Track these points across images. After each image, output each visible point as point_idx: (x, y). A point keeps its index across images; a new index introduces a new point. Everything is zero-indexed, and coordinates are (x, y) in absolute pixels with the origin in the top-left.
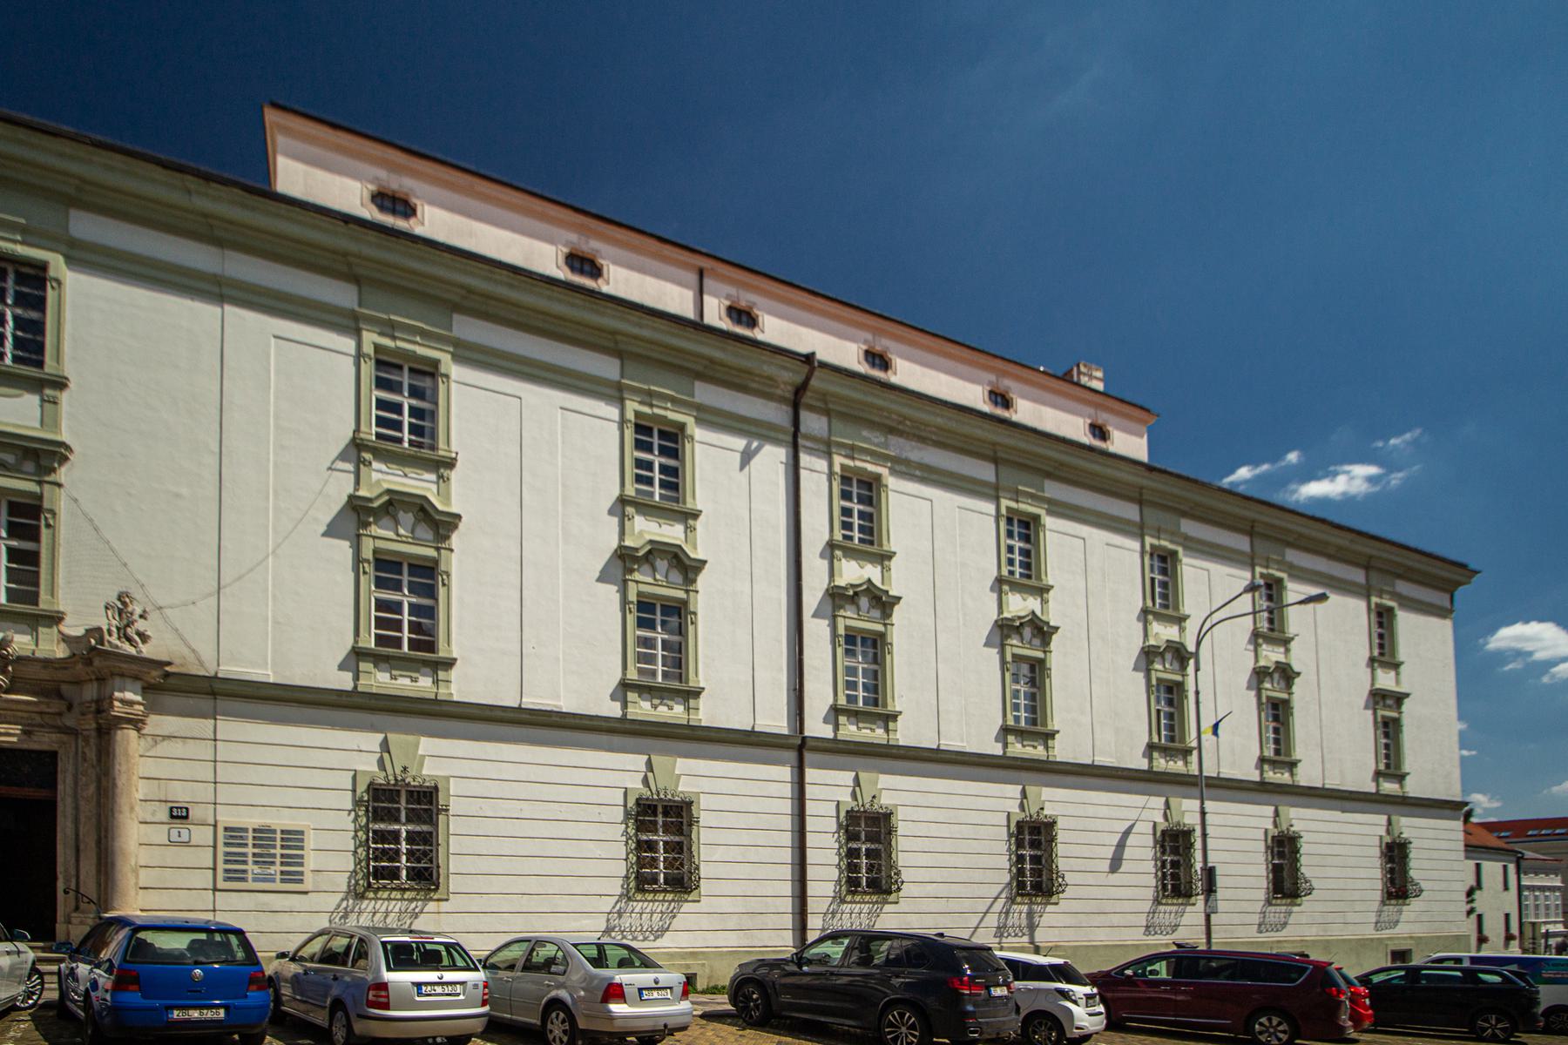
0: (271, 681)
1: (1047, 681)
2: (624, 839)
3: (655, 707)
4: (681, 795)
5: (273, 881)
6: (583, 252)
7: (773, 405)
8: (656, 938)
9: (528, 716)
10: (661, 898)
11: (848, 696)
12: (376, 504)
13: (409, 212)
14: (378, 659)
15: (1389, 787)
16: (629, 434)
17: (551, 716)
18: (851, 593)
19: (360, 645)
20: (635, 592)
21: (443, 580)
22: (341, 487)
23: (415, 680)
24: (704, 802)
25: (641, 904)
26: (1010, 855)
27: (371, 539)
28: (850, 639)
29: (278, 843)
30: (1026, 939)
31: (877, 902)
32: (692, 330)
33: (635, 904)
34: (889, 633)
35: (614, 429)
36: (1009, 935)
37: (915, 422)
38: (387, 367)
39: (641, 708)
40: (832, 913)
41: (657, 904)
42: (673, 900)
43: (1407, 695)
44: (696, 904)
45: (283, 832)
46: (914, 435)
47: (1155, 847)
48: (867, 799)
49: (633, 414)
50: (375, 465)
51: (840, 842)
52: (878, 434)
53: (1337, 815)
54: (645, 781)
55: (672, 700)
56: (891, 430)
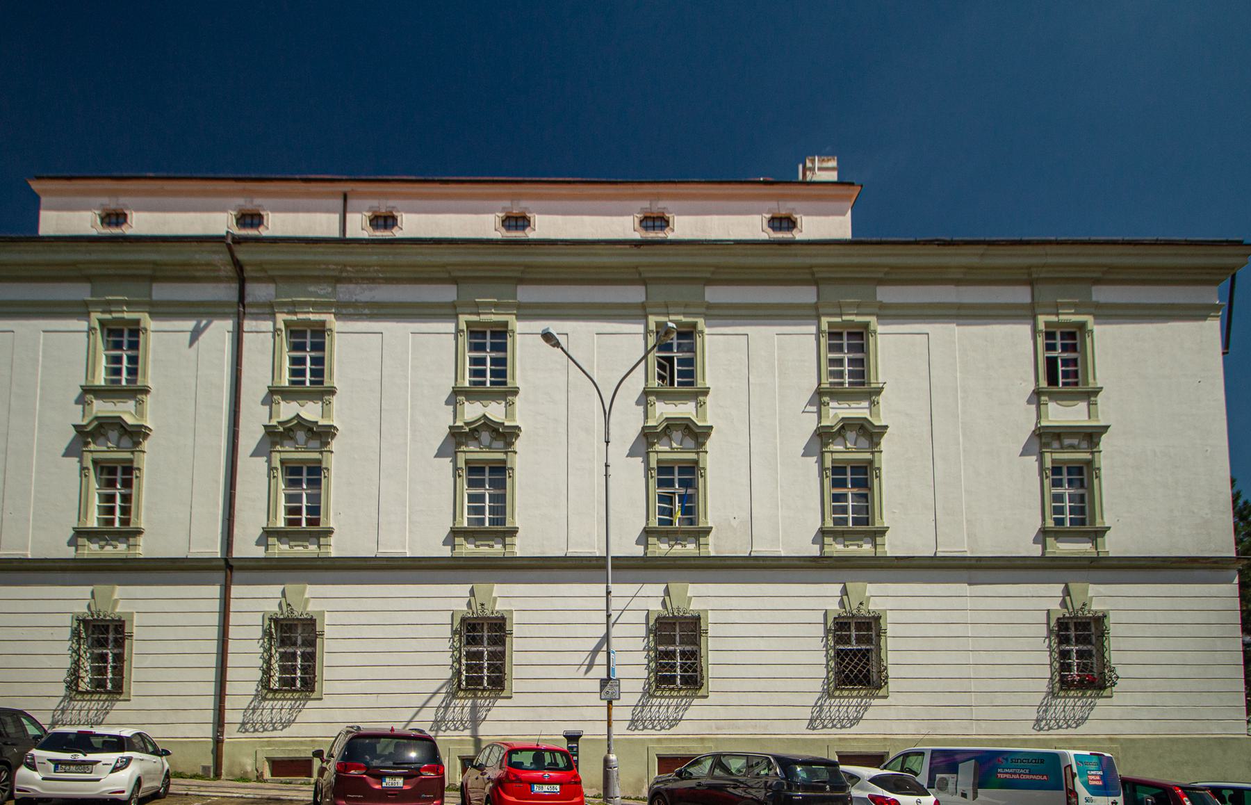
0: (408, 556)
1: (1096, 481)
2: (70, 652)
3: (102, 547)
4: (691, 612)
6: (248, 210)
7: (222, 286)
8: (671, 727)
9: (1128, 563)
10: (97, 698)
11: (1055, 519)
12: (89, 429)
13: (791, 225)
14: (834, 534)
16: (1041, 341)
17: (980, 561)
18: (467, 430)
19: (650, 526)
20: (1050, 460)
21: (876, 473)
22: (810, 424)
23: (306, 547)
24: (890, 617)
25: (80, 703)
26: (827, 651)
27: (830, 454)
28: (1056, 470)
30: (467, 732)
31: (299, 699)
32: (128, 244)
33: (76, 702)
34: (1096, 459)
35: (812, 340)
36: (448, 728)
37: (357, 266)
38: (476, 334)
39: (89, 549)
40: (253, 709)
41: (93, 703)
42: (106, 700)
43: (1105, 428)
44: (128, 702)
46: (363, 279)
47: (1048, 637)
48: (855, 605)
49: (97, 322)
50: (832, 404)
51: (264, 647)
52: (325, 286)
53: (964, 588)
54: (664, 604)
55: (117, 540)
56: (338, 280)
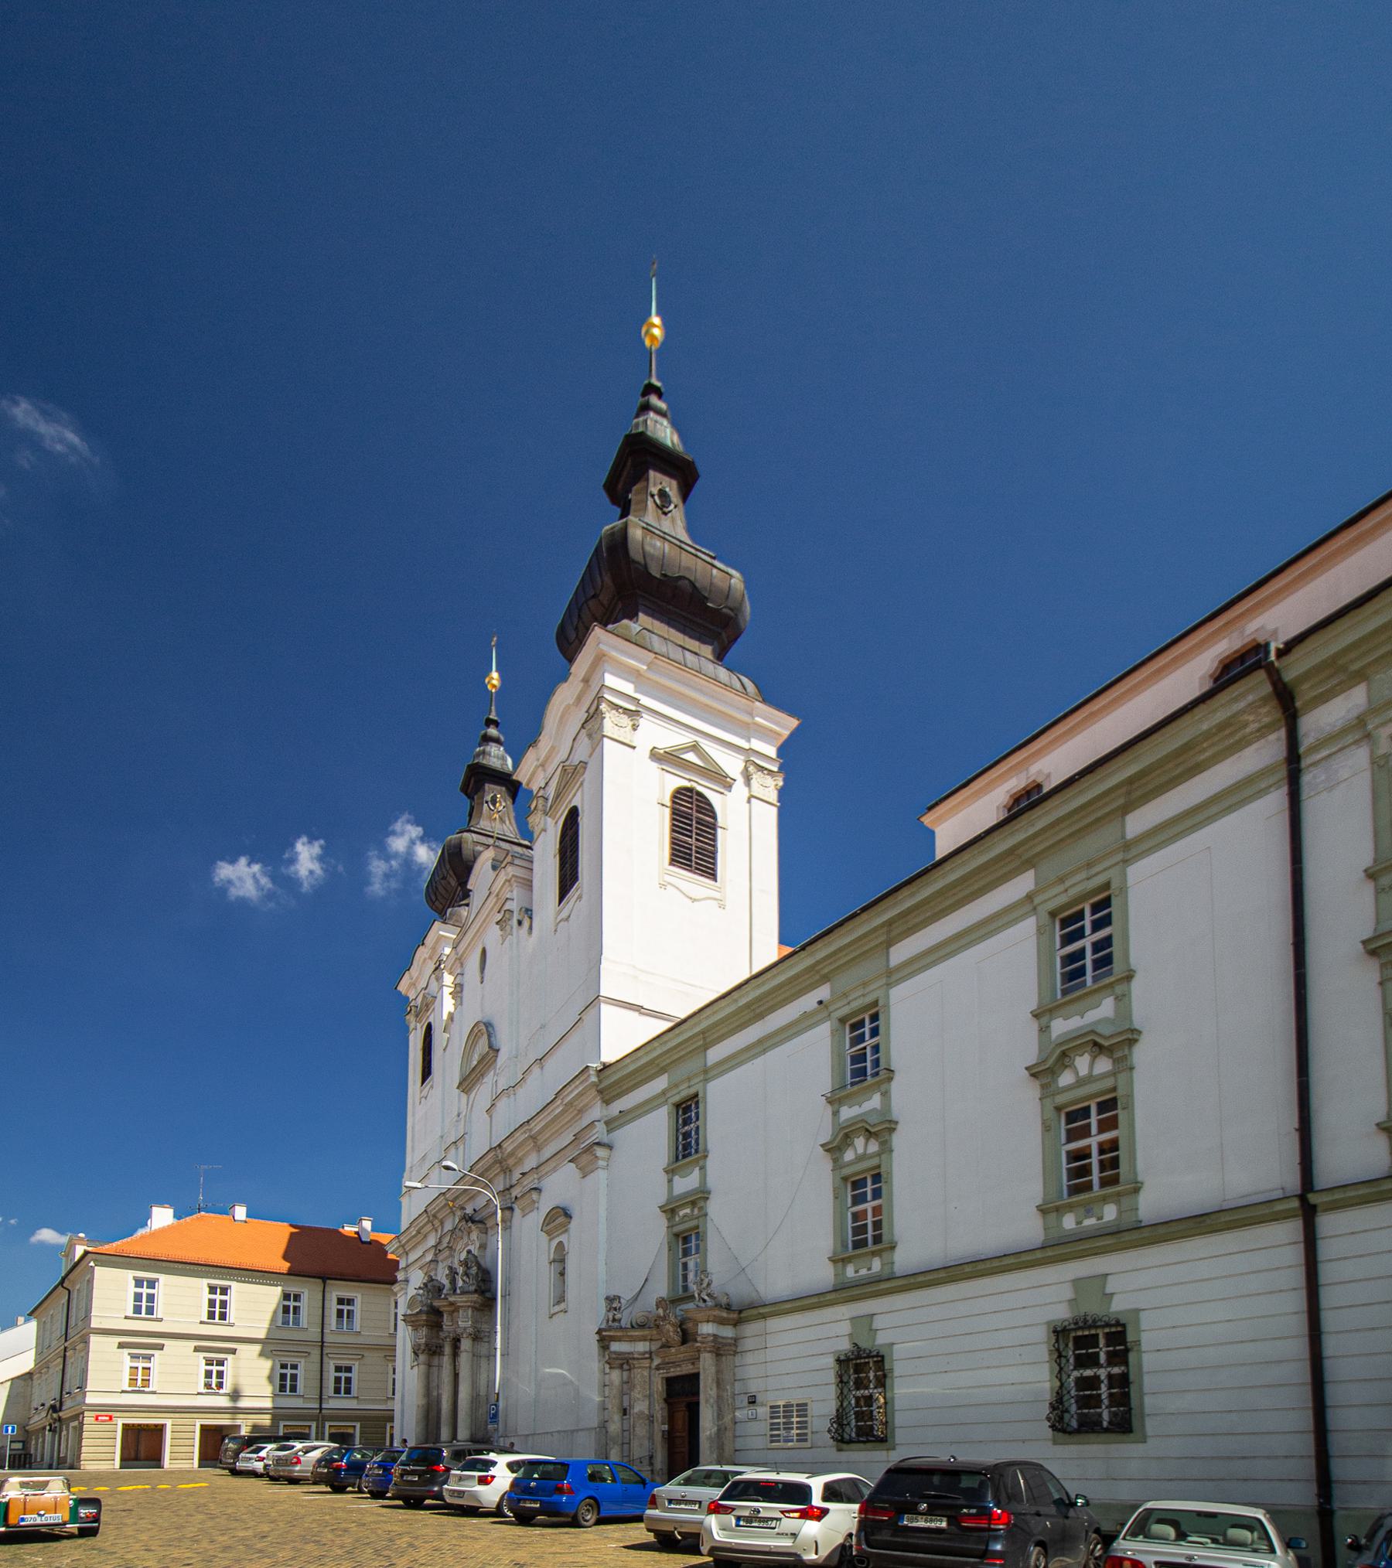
5: (792, 1441)
15: (686, 1295)
29: (795, 1414)
45: (797, 1405)
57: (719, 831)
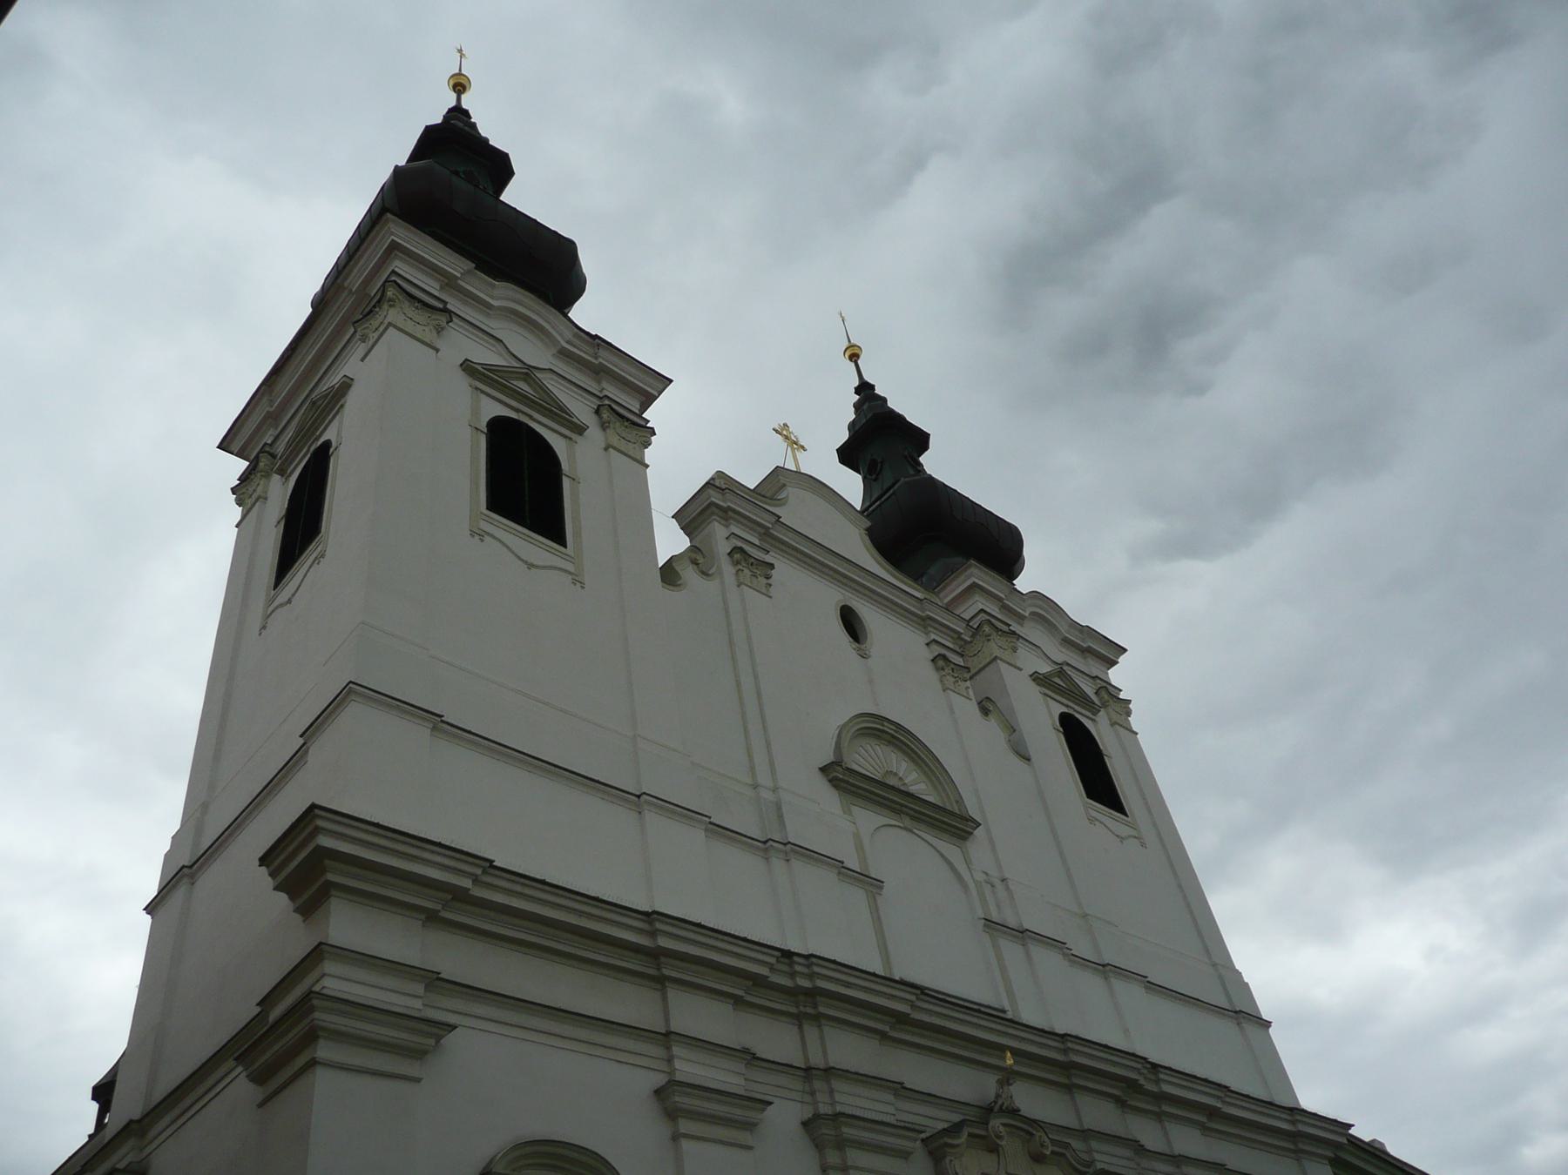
57: (566, 483)
